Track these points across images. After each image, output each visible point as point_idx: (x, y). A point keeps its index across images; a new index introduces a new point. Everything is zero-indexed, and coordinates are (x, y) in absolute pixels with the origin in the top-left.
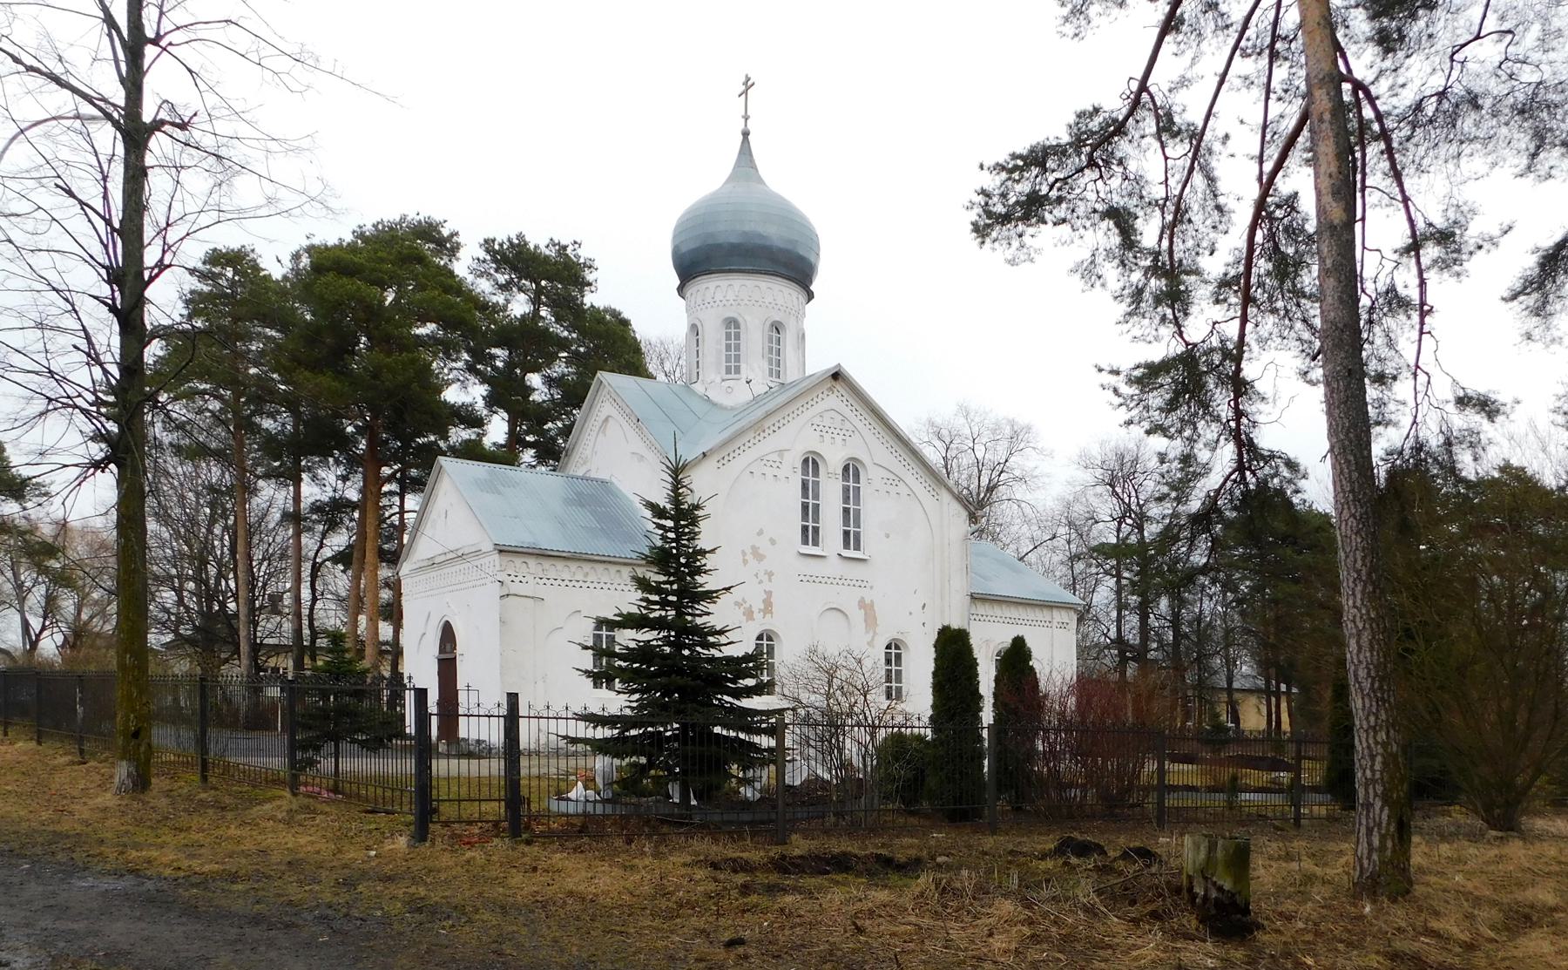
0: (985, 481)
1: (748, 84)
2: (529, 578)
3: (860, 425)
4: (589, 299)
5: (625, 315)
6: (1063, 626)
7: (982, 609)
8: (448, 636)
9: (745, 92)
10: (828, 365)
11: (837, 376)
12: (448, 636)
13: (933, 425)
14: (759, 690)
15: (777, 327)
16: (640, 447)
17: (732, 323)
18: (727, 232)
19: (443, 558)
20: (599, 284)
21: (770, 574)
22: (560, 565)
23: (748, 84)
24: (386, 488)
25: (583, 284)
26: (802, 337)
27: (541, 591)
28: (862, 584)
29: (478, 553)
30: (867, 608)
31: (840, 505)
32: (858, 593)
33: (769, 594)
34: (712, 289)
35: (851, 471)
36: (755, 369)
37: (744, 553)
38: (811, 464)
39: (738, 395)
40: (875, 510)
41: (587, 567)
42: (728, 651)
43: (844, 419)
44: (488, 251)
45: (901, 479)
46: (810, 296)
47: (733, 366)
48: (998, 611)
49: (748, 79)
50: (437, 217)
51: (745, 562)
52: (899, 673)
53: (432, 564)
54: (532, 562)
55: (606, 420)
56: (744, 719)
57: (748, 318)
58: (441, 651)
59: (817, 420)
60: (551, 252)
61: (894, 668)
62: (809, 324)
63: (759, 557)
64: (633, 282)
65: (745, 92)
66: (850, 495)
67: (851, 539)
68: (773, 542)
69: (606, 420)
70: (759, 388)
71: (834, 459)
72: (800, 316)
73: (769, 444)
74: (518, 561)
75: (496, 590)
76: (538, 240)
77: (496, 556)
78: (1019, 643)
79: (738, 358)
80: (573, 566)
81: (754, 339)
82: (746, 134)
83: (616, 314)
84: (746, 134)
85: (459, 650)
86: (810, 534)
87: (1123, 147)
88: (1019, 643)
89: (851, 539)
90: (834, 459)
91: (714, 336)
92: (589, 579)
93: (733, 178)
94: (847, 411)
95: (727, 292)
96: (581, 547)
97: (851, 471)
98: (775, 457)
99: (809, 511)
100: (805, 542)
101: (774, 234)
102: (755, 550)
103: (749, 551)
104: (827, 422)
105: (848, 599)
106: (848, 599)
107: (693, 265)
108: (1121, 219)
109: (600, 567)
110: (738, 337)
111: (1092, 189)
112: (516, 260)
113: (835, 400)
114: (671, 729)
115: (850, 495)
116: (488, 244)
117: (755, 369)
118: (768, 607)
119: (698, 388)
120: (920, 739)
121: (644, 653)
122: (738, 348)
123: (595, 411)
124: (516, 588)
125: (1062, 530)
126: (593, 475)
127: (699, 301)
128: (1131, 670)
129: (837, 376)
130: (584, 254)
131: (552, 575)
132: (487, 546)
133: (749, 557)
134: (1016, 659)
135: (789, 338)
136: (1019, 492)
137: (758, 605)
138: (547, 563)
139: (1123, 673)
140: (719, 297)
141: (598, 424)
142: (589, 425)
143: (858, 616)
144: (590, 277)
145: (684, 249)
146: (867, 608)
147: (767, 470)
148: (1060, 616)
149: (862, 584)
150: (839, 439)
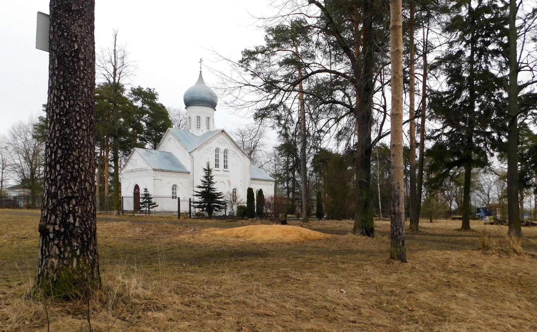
0: (253, 145)
1: (201, 61)
4: (157, 102)
5: (164, 105)
6: (271, 185)
7: (253, 181)
10: (221, 128)
13: (239, 130)
14: (222, 198)
15: (208, 118)
16: (180, 146)
17: (198, 117)
18: (197, 96)
22: (165, 173)
23: (201, 61)
25: (155, 98)
26: (214, 120)
27: (162, 178)
28: (228, 176)
30: (229, 181)
32: (227, 178)
35: (226, 151)
36: (203, 127)
38: (217, 150)
39: (200, 133)
40: (231, 160)
41: (171, 173)
42: (216, 192)
46: (215, 110)
47: (199, 127)
48: (257, 182)
52: (176, 192)
53: (132, 171)
54: (160, 172)
56: (219, 202)
58: (134, 191)
60: (147, 91)
62: (215, 117)
64: (171, 100)
67: (226, 167)
70: (205, 132)
71: (222, 149)
72: (213, 114)
73: (208, 146)
74: (157, 172)
75: (153, 178)
77: (153, 171)
78: (261, 190)
80: (168, 173)
81: (203, 121)
82: (201, 72)
83: (161, 105)
84: (201, 72)
87: (278, 109)
88: (261, 190)
89: (226, 167)
90: (222, 149)
93: (197, 83)
94: (225, 139)
95: (196, 110)
96: (163, 168)
97: (226, 151)
101: (208, 97)
105: (225, 179)
107: (189, 102)
108: (279, 118)
111: (273, 113)
113: (222, 136)
114: (206, 204)
117: (203, 127)
119: (191, 131)
120: (244, 206)
121: (203, 192)
124: (157, 178)
125: (273, 158)
126: (166, 151)
128: (291, 195)
129: (222, 131)
130: (155, 91)
132: (150, 168)
134: (260, 192)
135: (211, 121)
136: (262, 148)
138: (163, 172)
139: (289, 195)
140: (195, 111)
142: (166, 138)
143: (227, 183)
145: (188, 99)
146: (229, 181)
148: (270, 183)
149: (228, 176)
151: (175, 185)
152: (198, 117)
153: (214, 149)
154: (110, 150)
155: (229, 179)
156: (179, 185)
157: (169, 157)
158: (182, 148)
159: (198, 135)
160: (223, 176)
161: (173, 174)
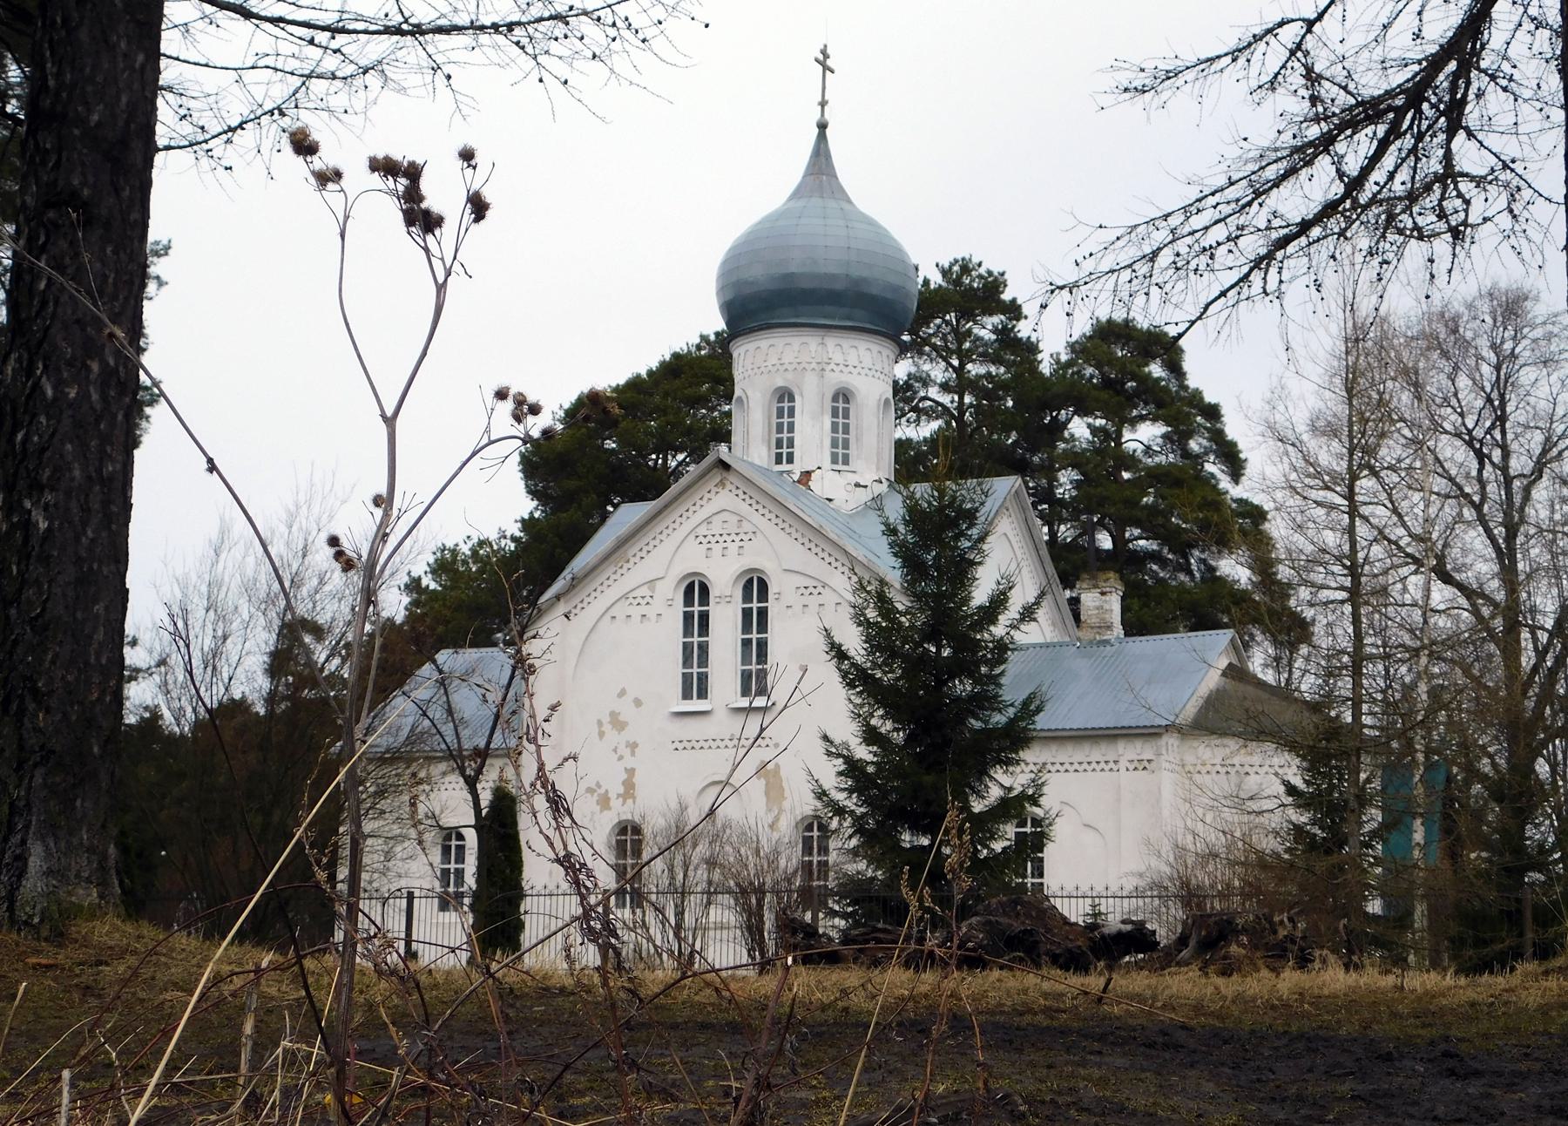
33: (631, 772)
37: (600, 723)
51: (601, 734)
68: (638, 703)
82: (822, 126)
84: (822, 126)
86: (695, 686)
102: (614, 716)
133: (607, 728)
137: (615, 788)
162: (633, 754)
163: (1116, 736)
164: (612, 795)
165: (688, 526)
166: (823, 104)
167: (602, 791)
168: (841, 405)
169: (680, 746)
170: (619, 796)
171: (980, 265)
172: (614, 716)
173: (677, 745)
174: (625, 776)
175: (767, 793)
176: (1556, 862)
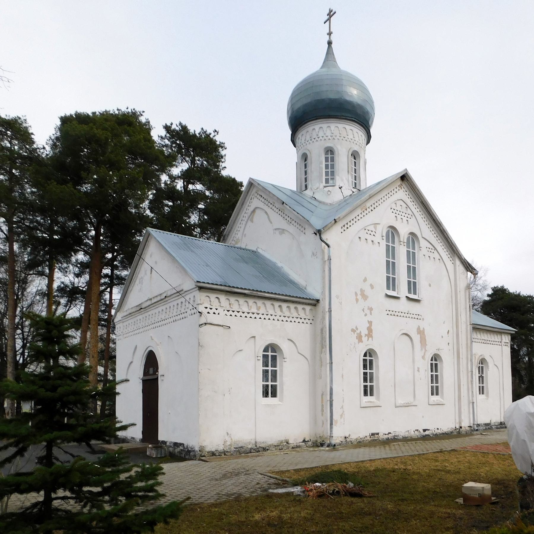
1: (331, 14)
2: (220, 310)
3: (415, 211)
8: (151, 361)
9: (329, 19)
11: (404, 178)
12: (151, 361)
19: (149, 303)
20: (226, 158)
21: (371, 309)
23: (331, 14)
24: (102, 281)
28: (418, 317)
29: (179, 293)
30: (421, 332)
31: (406, 264)
33: (370, 323)
34: (317, 130)
37: (356, 294)
38: (392, 232)
39: (336, 196)
43: (408, 207)
44: (168, 132)
45: (435, 249)
46: (369, 137)
47: (331, 174)
49: (331, 11)
50: (138, 109)
51: (357, 300)
53: (140, 309)
54: (223, 298)
55: (254, 211)
57: (339, 147)
58: (146, 373)
59: (394, 206)
61: (270, 368)
63: (365, 297)
65: (329, 19)
66: (411, 257)
67: (412, 287)
68: (372, 287)
69: (254, 211)
70: (347, 192)
71: (404, 231)
76: (194, 128)
79: (333, 173)
81: (342, 160)
82: (330, 43)
84: (330, 43)
85: (161, 372)
86: (391, 283)
89: (412, 287)
91: (318, 161)
92: (261, 312)
94: (408, 201)
96: (235, 281)
98: (372, 228)
99: (391, 266)
100: (388, 288)
102: (362, 291)
103: (359, 293)
104: (399, 208)
106: (411, 327)
109: (268, 303)
110: (333, 160)
112: (181, 137)
115: (411, 257)
116: (167, 128)
117: (343, 178)
118: (370, 335)
122: (333, 166)
123: (246, 206)
127: (308, 138)
129: (404, 178)
130: (218, 139)
131: (235, 307)
132: (188, 285)
133: (359, 297)
137: (365, 332)
140: (321, 134)
141: (247, 216)
142: (242, 214)
143: (416, 338)
144: (223, 153)
147: (368, 237)
148: (496, 338)
149: (418, 317)
150: (405, 219)
151: (272, 348)
152: (330, 151)
153: (382, 230)
154: (354, 486)
155: (422, 325)
156: (285, 346)
157: (253, 258)
158: (291, 229)
159: (328, 201)
160: (407, 315)
161: (268, 307)
162: (371, 314)
163: (504, 333)
164: (363, 334)
165: (410, 204)
166: (330, 34)
167: (358, 332)
168: (329, 156)
169: (389, 313)
170: (366, 335)
171: (172, 124)
172: (362, 291)
173: (388, 312)
174: (368, 325)
175: (421, 342)
176: (167, 206)
